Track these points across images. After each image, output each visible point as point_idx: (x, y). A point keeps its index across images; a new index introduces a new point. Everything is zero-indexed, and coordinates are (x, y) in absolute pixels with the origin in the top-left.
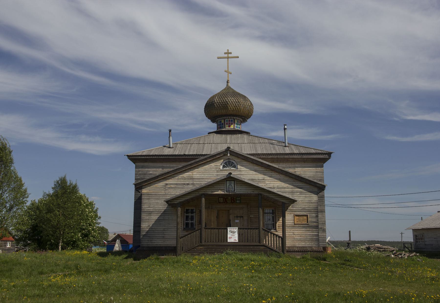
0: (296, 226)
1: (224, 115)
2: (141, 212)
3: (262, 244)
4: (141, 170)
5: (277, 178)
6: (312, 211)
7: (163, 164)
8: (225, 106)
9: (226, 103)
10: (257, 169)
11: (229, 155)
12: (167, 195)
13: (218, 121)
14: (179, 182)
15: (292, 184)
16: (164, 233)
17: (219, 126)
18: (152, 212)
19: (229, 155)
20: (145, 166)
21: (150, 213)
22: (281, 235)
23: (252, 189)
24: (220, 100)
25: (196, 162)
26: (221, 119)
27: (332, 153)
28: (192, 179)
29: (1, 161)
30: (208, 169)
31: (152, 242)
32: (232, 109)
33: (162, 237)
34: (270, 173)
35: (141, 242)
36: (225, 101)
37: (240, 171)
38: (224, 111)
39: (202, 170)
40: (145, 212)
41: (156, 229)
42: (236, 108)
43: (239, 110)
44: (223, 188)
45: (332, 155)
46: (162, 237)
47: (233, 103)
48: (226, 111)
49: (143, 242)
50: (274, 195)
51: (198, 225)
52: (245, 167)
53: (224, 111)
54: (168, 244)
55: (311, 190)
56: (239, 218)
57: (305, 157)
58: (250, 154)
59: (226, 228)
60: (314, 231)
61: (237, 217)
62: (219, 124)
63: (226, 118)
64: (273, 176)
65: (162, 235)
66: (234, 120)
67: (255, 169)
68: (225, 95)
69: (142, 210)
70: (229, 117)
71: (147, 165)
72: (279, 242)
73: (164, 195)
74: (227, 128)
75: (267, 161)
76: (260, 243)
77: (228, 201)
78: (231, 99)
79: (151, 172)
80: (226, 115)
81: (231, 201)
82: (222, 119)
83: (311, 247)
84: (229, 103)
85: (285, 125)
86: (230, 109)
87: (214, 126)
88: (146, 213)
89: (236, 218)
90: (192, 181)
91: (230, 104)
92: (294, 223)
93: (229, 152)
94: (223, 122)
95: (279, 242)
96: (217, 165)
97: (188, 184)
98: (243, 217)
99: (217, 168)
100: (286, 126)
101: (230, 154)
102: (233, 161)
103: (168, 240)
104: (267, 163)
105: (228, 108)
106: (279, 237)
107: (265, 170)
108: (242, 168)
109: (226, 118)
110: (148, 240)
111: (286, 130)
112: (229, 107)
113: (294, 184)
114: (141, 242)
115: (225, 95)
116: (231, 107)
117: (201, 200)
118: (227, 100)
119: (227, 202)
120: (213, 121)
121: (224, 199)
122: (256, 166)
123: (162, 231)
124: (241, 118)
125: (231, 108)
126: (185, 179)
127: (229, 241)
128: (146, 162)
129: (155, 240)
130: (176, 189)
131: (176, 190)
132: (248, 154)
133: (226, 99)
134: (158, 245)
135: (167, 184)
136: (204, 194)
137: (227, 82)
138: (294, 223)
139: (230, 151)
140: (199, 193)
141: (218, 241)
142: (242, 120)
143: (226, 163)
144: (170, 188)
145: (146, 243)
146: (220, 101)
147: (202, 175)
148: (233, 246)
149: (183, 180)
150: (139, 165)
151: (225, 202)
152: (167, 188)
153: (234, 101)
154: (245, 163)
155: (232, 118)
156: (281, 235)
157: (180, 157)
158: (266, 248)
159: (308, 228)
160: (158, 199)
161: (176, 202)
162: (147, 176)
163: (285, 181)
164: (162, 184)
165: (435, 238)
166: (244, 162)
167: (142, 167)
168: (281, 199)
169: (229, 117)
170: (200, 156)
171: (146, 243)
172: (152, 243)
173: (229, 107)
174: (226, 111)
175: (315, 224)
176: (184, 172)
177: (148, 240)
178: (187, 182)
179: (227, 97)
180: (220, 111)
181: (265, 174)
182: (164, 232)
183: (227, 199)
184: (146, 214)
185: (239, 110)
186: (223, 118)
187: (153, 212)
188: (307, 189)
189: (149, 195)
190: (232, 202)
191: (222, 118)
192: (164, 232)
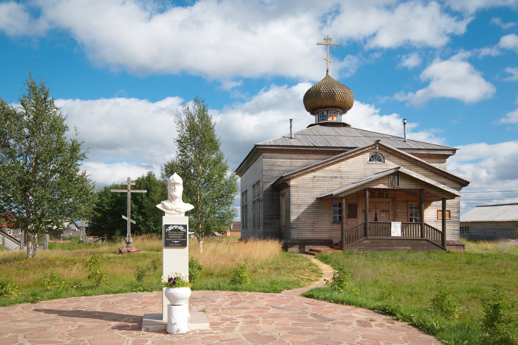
0: (438, 220)
1: (329, 106)
2: (290, 204)
3: (424, 239)
4: (269, 161)
5: (422, 173)
6: (455, 206)
7: (291, 155)
8: (332, 95)
9: (333, 94)
10: (403, 164)
11: (377, 148)
12: (315, 187)
13: (319, 112)
14: (327, 175)
15: (436, 180)
16: (314, 226)
17: (321, 117)
18: (301, 205)
19: (377, 148)
20: (273, 157)
21: (299, 206)
22: (441, 230)
23: (415, 184)
24: (326, 89)
25: (345, 155)
26: (324, 111)
27: (457, 149)
28: (340, 171)
29: (3, 147)
30: (356, 162)
31: (302, 235)
32: (339, 100)
33: (312, 230)
34: (416, 168)
35: (291, 235)
36: (332, 91)
37: (387, 165)
38: (331, 102)
39: (350, 163)
40: (294, 204)
41: (305, 222)
42: (343, 100)
43: (345, 102)
44: (387, 183)
45: (456, 150)
46: (312, 230)
47: (341, 94)
48: (333, 102)
49: (293, 235)
50: (436, 191)
51: (346, 218)
52: (392, 161)
53: (331, 102)
54: (317, 237)
55: (454, 186)
56: (384, 212)
57: (431, 152)
58: (400, 149)
59: (390, 222)
60: (456, 226)
61: (383, 211)
62: (321, 116)
63: (330, 109)
64: (419, 171)
65: (311, 228)
66: (337, 111)
67: (401, 164)
68: (327, 85)
69: (291, 203)
70: (333, 109)
71: (275, 156)
72: (439, 237)
73: (312, 187)
74: (330, 119)
75: (415, 156)
76: (422, 238)
77: (375, 195)
78: (338, 89)
79: (279, 164)
80: (331, 106)
81: (378, 195)
82: (325, 111)
83: (453, 241)
84: (336, 93)
85: (405, 119)
86: (337, 100)
87: (312, 119)
88: (295, 205)
89: (382, 212)
90: (340, 174)
91: (337, 95)
92: (437, 218)
93: (377, 145)
94: (325, 113)
95: (439, 237)
96: (364, 159)
97: (336, 177)
98: (388, 211)
99: (365, 161)
100: (405, 121)
101: (379, 148)
102: (380, 156)
103: (317, 234)
104: (416, 158)
105: (335, 99)
106: (439, 232)
107: (411, 165)
108: (389, 162)
109: (330, 109)
110: (298, 233)
111: (406, 125)
112: (337, 98)
113: (438, 180)
114: (291, 235)
115: (327, 85)
116: (338, 98)
117: (144, 189)
118: (335, 91)
119: (374, 196)
120: (313, 112)
121: (371, 193)
122: (403, 161)
123: (311, 224)
124: (342, 110)
125: (338, 99)
126: (332, 171)
127: (393, 235)
128: (274, 153)
129: (305, 233)
130: (324, 182)
131: (324, 183)
132: (397, 148)
133: (333, 89)
134: (308, 238)
135: (315, 177)
136: (369, 188)
137: (327, 71)
138: (437, 218)
139: (380, 144)
140: (363, 187)
141: (363, 233)
142: (342, 111)
143: (372, 157)
144: (319, 181)
145: (296, 236)
146: (327, 91)
147: (350, 169)
148: (397, 239)
149: (330, 173)
150: (266, 156)
151: (372, 197)
152: (315, 181)
153: (342, 92)
154: (392, 157)
155: (335, 110)
156: (441, 230)
157: (310, 149)
158: (428, 242)
159: (450, 223)
160: (306, 192)
161: (342, 195)
162: (275, 167)
163: (429, 176)
164: (310, 175)
165: (483, 230)
166: (391, 156)
167: (270, 158)
168: (443, 194)
169: (333, 109)
170: (348, 149)
171: (296, 236)
172: (302, 236)
173: (337, 98)
174: (333, 102)
175: (457, 219)
176: (332, 164)
177: (298, 233)
178: (335, 175)
179: (334, 87)
180: (327, 102)
181: (411, 169)
182: (314, 225)
183: (374, 193)
184: (295, 206)
185: (345, 102)
186: (331, 109)
187: (302, 204)
188: (451, 185)
189: (298, 188)
190: (379, 196)
191: (324, 109)
192: (314, 225)
